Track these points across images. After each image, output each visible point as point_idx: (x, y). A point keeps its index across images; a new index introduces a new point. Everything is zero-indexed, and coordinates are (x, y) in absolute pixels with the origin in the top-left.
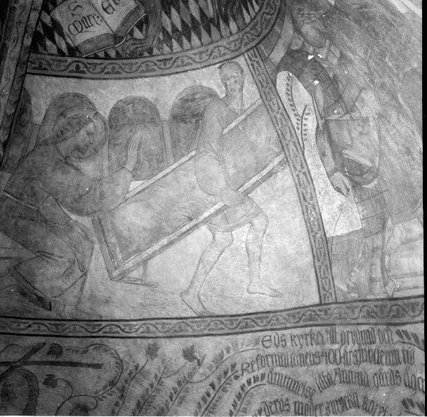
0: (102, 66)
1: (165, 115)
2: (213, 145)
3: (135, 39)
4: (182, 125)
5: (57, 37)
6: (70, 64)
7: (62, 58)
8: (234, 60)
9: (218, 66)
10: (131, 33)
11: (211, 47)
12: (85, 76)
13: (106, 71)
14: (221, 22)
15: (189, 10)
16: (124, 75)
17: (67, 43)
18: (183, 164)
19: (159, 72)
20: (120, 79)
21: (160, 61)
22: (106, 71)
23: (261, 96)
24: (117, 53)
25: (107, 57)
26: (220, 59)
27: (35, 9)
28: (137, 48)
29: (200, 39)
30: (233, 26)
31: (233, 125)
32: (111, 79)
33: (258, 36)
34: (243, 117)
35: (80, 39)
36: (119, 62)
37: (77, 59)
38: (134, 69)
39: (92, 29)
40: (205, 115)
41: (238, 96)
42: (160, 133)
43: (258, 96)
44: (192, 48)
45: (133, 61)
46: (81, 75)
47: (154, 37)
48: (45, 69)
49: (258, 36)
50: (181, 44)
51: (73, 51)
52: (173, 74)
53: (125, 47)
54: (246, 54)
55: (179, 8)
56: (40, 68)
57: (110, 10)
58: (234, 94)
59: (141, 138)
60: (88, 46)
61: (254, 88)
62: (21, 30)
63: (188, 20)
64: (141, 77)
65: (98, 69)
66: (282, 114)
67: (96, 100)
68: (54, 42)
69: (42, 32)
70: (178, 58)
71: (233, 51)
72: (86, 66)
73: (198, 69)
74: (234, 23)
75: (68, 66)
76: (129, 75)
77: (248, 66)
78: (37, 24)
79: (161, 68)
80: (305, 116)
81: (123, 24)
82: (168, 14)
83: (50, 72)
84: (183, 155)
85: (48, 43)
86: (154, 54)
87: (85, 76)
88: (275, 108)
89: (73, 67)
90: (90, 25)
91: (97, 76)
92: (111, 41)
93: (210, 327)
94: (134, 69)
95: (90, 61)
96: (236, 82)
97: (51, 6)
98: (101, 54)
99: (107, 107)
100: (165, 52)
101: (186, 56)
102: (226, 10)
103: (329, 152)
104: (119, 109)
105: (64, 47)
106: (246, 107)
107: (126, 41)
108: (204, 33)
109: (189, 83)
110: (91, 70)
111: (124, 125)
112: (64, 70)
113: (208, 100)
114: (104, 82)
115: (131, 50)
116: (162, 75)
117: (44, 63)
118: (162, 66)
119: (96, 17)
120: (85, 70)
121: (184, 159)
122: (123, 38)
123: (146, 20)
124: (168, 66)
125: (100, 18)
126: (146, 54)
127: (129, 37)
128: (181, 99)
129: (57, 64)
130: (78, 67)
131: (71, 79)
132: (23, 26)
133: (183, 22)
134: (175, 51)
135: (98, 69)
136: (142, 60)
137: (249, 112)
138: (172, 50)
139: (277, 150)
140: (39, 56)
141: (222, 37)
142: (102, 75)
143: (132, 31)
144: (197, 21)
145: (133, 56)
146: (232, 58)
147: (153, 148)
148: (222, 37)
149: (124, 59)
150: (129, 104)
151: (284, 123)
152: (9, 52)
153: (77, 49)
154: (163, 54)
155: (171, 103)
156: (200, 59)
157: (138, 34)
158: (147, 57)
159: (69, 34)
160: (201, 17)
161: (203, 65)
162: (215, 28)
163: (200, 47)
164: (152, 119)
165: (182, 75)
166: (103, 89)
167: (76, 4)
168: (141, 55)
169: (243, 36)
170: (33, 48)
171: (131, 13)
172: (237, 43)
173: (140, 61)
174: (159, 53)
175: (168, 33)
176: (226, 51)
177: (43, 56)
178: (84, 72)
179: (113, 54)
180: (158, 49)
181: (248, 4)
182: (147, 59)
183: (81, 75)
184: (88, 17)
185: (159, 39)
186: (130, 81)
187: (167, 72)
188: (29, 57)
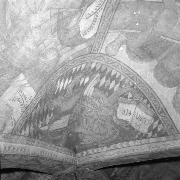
0: (154, 102)
1: (155, 63)
2: (150, 32)
3: (133, 95)
4: (153, 52)
5: (154, 127)
6: (162, 116)
7: (162, 121)
8: (106, 53)
9: (114, 57)
10: (131, 98)
11: (110, 65)
12: (163, 107)
13: (154, 100)
14: (97, 70)
15: (105, 82)
16: (151, 91)
17: (154, 122)
18: (172, 39)
19: (138, 78)
20: (154, 91)
21: (133, 80)
22: (154, 100)
23: (107, 33)
24: (144, 99)
25: (148, 102)
26: (111, 58)
27: (149, 141)
28: (135, 92)
29: (111, 71)
30: (93, 66)
31: (132, 31)
32: (157, 95)
33: (85, 57)
34: (124, 30)
35: (149, 118)
36: (147, 96)
37: (158, 115)
38: (145, 88)
39: (141, 115)
40: (139, 46)
41: (118, 40)
42: (165, 59)
43: (109, 34)
44: (118, 71)
45: (142, 91)
46: (164, 109)
47: (126, 88)
48: (172, 126)
49: (85, 57)
50: (120, 76)
51: (156, 118)
52: (134, 72)
53: (139, 97)
54: (98, 52)
55: (107, 87)
56: (172, 128)
57: (129, 112)
58: (119, 42)
59: (175, 66)
60: (149, 112)
61: (107, 38)
62: (160, 144)
63: (109, 80)
64: (147, 84)
65: (156, 103)
66: (104, 19)
67: (171, 97)
68: (157, 127)
69: (156, 134)
70: (126, 74)
71: (103, 57)
72: (159, 109)
73: (123, 63)
74: (92, 66)
75: (164, 117)
76: (149, 89)
77: (101, 48)
78: (154, 137)
79: (136, 78)
80: (92, 13)
81: (130, 104)
82: (113, 89)
83: (171, 123)
84: (167, 41)
85: (159, 129)
86: (133, 84)
87: (163, 107)
88: (105, 24)
89: (163, 114)
90: (140, 116)
91: (159, 102)
92: (141, 104)
93: (142, 85)
94: (145, 88)
95: (155, 109)
96: (113, 46)
97: (144, 135)
98: (149, 105)
99: (171, 90)
100: (128, 80)
101: (123, 71)
102: (91, 72)
104: (168, 84)
105: (157, 122)
106: (119, 33)
107: (136, 98)
108: (108, 71)
109: (132, 62)
110: (159, 106)
111: (174, 78)
112: (166, 117)
113: (132, 49)
114: (160, 98)
115: (138, 94)
116: (138, 75)
117: (169, 128)
118: (135, 78)
119: (136, 116)
120: (160, 109)
121: (170, 40)
122: (136, 100)
123: (122, 96)
124: (133, 75)
125: (135, 114)
126: (135, 87)
127: (134, 98)
128: (142, 61)
129: (166, 122)
130: (161, 112)
131: (169, 113)
132: (157, 144)
133: (111, 82)
134: (125, 77)
135: (156, 103)
136: (138, 87)
137: (120, 31)
138: (125, 78)
139: (123, 5)
140: (167, 131)
141: (102, 65)
142: (158, 100)
143: (131, 98)
144: (106, 77)
145: (140, 92)
146: (106, 55)
147: (175, 58)
148: (102, 65)
149: (144, 95)
150: (162, 81)
151: (107, 15)
152: (172, 146)
153: (153, 117)
154: (130, 80)
155: (147, 64)
156: (118, 65)
157: (130, 95)
158: (136, 86)
159: (150, 123)
160: (103, 77)
161: (120, 63)
162: (102, 69)
163: (114, 69)
164: (161, 67)
165: (131, 67)
166: (164, 97)
167: (136, 126)
168: (137, 89)
169: (92, 60)
170: (165, 135)
171: (124, 103)
172: (98, 59)
173: (140, 88)
174: (131, 82)
175: (120, 84)
176: (105, 59)
177: (166, 129)
178: (162, 109)
179: (145, 101)
180: (129, 84)
181: (77, 71)
182: (137, 85)
183: (164, 109)
184: (137, 119)
185: (125, 86)
186: (151, 87)
187: (135, 74)
188: (171, 135)
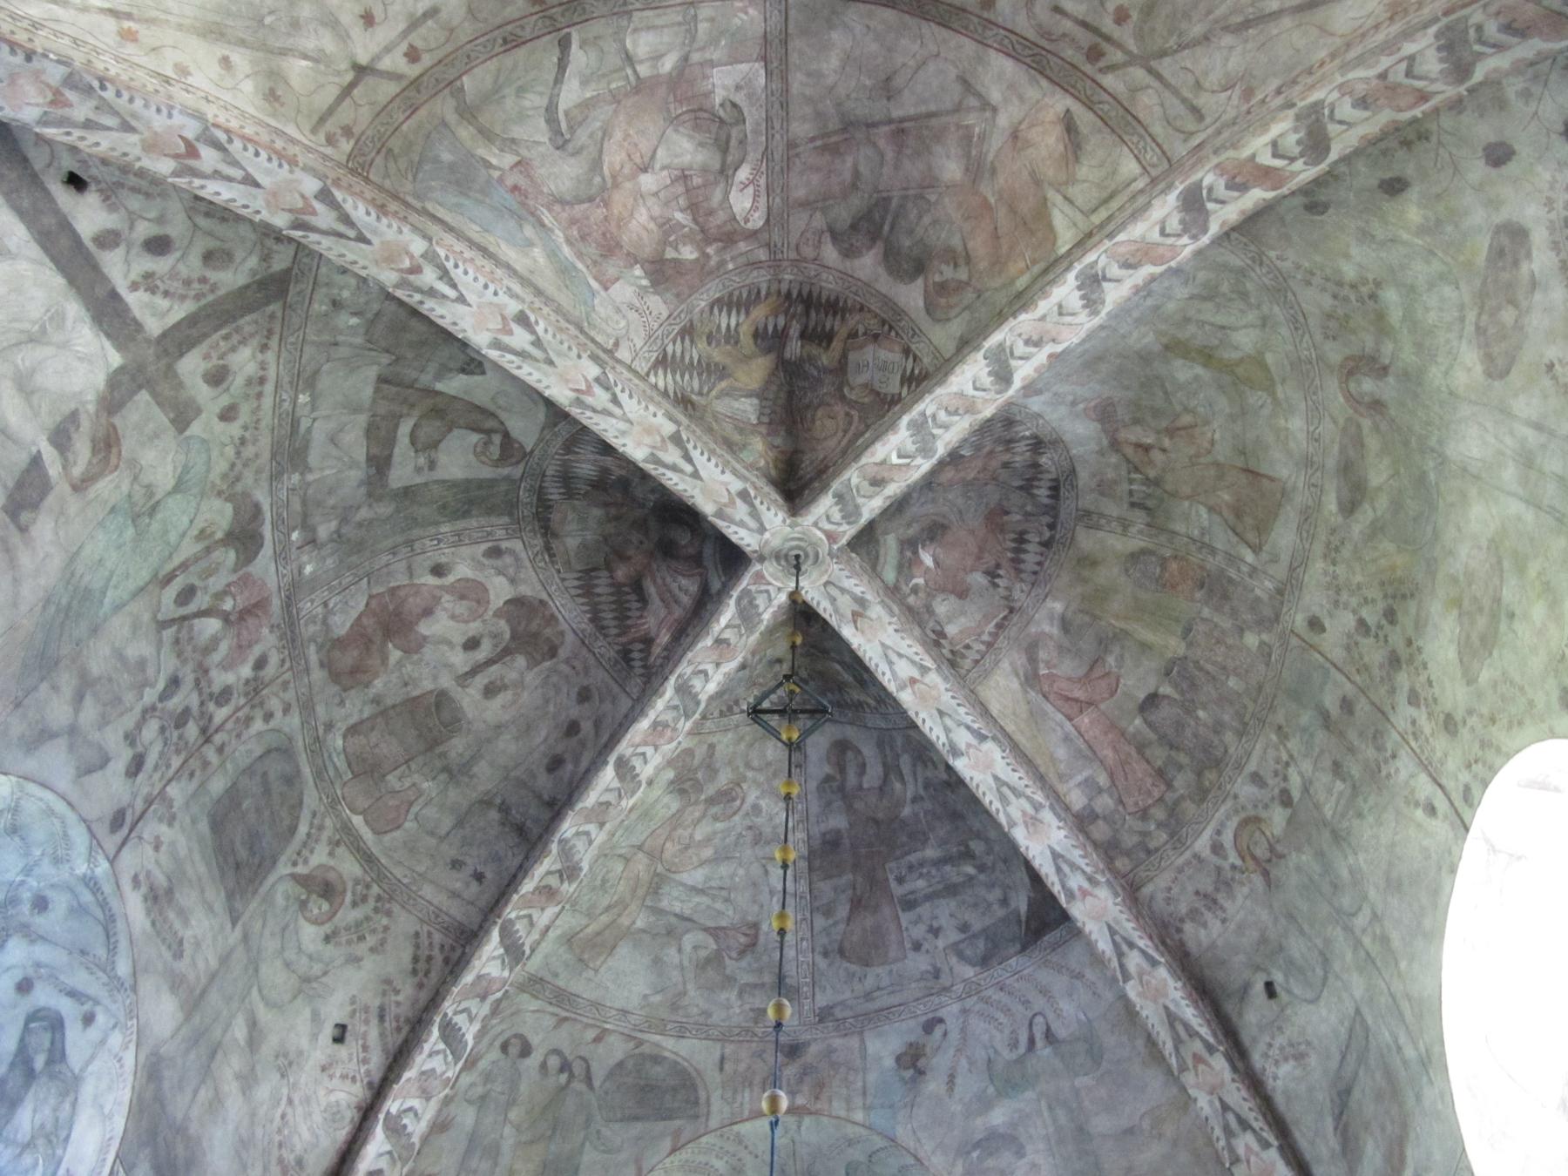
103: (733, 143)
